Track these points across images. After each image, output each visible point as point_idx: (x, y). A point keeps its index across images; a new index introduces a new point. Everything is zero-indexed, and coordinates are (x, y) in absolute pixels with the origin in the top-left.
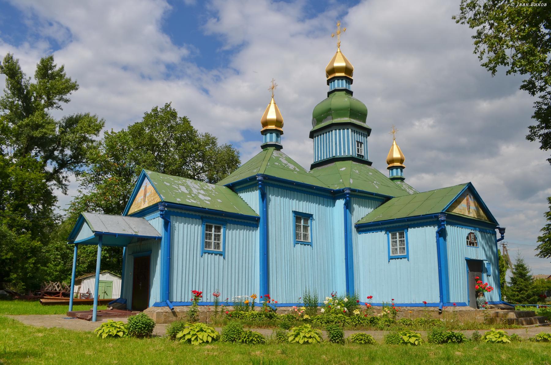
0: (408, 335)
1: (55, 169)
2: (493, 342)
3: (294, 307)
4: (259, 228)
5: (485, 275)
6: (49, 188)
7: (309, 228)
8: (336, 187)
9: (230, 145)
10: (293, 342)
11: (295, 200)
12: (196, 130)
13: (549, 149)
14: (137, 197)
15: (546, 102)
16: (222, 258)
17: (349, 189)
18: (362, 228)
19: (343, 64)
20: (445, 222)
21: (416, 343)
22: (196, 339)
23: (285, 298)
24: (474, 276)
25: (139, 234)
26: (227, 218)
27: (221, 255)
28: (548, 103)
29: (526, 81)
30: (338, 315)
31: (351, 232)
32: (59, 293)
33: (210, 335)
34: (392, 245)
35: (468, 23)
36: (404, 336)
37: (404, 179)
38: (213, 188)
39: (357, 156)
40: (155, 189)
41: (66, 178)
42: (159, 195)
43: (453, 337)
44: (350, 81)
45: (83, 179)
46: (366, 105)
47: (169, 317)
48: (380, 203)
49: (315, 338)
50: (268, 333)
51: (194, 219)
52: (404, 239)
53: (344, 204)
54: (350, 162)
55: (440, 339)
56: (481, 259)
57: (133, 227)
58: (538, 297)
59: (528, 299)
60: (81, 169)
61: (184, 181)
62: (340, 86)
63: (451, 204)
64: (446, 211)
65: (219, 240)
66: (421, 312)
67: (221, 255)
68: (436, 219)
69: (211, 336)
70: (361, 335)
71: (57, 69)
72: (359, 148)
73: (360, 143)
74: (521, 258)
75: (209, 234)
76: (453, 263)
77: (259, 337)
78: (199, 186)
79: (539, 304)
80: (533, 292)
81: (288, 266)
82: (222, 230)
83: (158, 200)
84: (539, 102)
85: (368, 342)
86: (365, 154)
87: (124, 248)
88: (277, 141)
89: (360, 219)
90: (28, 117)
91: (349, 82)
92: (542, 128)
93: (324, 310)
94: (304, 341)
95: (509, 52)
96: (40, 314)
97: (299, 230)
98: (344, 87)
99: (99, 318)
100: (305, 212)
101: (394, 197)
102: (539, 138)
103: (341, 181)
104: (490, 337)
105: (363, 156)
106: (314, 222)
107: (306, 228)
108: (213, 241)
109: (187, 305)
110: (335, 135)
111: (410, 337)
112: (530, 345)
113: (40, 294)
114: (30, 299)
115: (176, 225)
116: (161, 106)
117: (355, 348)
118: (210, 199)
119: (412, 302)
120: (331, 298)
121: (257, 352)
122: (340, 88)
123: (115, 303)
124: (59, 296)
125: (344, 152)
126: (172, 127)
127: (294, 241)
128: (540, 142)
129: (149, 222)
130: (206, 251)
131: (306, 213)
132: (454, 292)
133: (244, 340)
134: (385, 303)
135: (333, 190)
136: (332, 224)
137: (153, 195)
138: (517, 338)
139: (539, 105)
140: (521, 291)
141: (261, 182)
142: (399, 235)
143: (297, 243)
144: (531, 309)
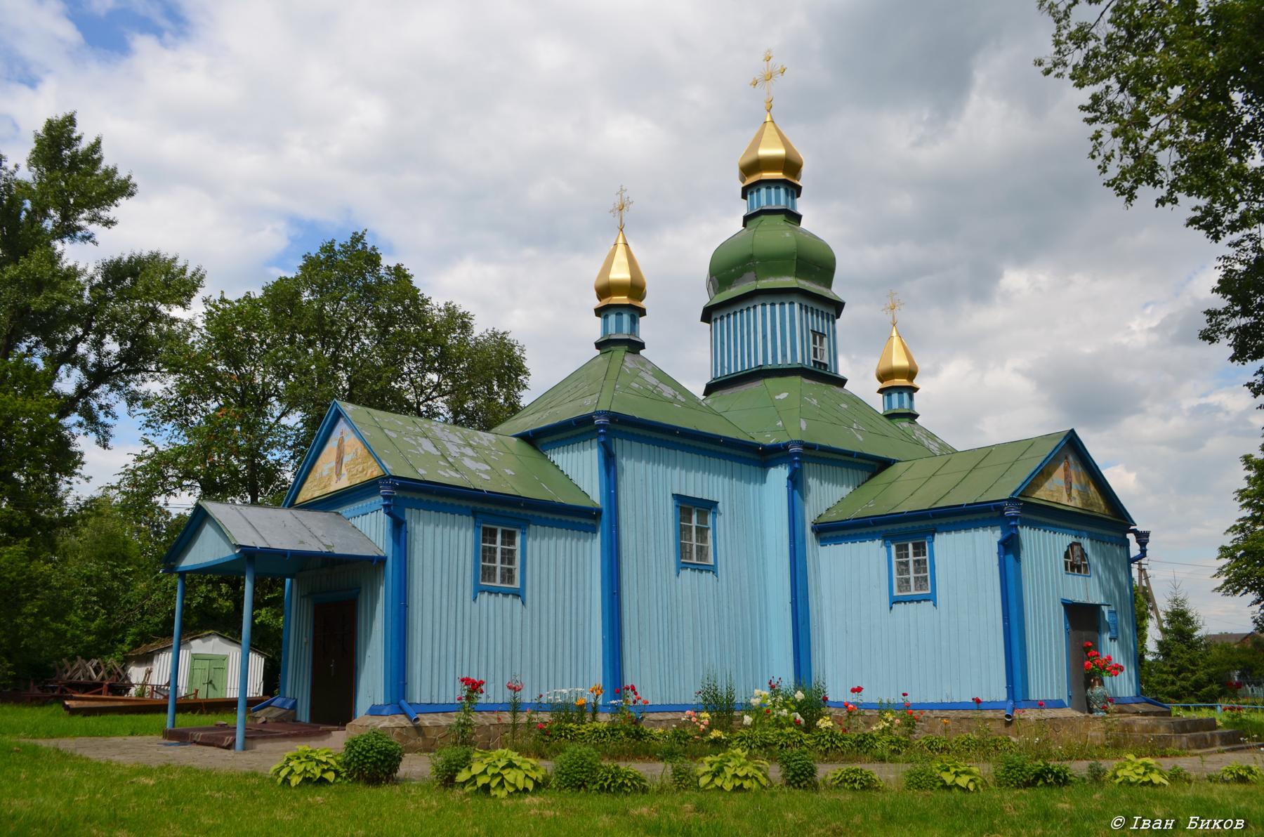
0: (953, 770)
1: (80, 387)
2: (1131, 784)
3: (688, 712)
4: (599, 534)
6: (66, 433)
7: (710, 533)
8: (770, 439)
9: (504, 333)
10: (710, 787)
11: (678, 469)
12: (426, 296)
13: (1249, 361)
14: (319, 463)
15: (1243, 258)
16: (519, 601)
17: (800, 444)
18: (830, 531)
19: (780, 152)
20: (1018, 520)
21: (971, 786)
22: (501, 785)
23: (659, 693)
25: (337, 551)
26: (529, 513)
28: (1249, 260)
29: (1200, 209)
30: (784, 728)
32: (99, 685)
33: (530, 775)
34: (898, 570)
35: (1072, 77)
36: (944, 773)
37: (916, 416)
38: (490, 441)
39: (812, 365)
40: (366, 445)
41: (107, 409)
42: (378, 461)
43: (1047, 774)
44: (795, 191)
45: (151, 413)
46: (834, 252)
47: (407, 738)
48: (867, 474)
49: (756, 779)
50: (654, 771)
51: (457, 515)
52: (924, 557)
53: (788, 478)
54: (797, 380)
55: (1021, 777)
56: (1097, 603)
57: (319, 533)
58: (1220, 687)
59: (1196, 690)
60: (143, 389)
61: (425, 425)
62: (773, 203)
63: (1031, 479)
64: (1020, 495)
65: (511, 562)
66: (966, 722)
68: (997, 514)
69: (531, 779)
70: (853, 771)
71: (83, 146)
72: (818, 346)
73: (818, 335)
74: (1181, 597)
75: (490, 548)
76: (1035, 612)
77: (635, 778)
78: (460, 438)
79: (1222, 704)
80: (1208, 674)
81: (665, 620)
82: (518, 539)
83: (374, 472)
84: (1228, 258)
85: (868, 785)
86: (830, 361)
87: (288, 581)
89: (824, 513)
90: (16, 262)
91: (792, 192)
92: (1234, 315)
93: (751, 719)
94: (734, 786)
95: (1167, 158)
96: (98, 736)
97: (688, 537)
98: (782, 205)
99: (249, 742)
100: (700, 497)
101: (899, 461)
102: (1227, 337)
103: (780, 423)
104: (1126, 773)
105: (825, 365)
106: (719, 519)
107: (702, 532)
108: (498, 564)
109: (444, 709)
110: (760, 316)
111: (957, 774)
112: (1211, 790)
113: (53, 689)
114: (32, 699)
116: (343, 239)
117: (846, 797)
119: (945, 700)
120: (766, 693)
121: (642, 809)
122: (773, 206)
123: (268, 709)
124: (100, 693)
125: (784, 355)
126: (368, 288)
128: (1230, 345)
129: (353, 521)
131: (702, 499)
132: (1038, 677)
133: (606, 785)
134: (885, 701)
135: (763, 446)
137: (360, 460)
138: (1183, 776)
139: (1229, 263)
140: (1180, 672)
142: (914, 549)
143: (682, 568)
144: (1204, 714)
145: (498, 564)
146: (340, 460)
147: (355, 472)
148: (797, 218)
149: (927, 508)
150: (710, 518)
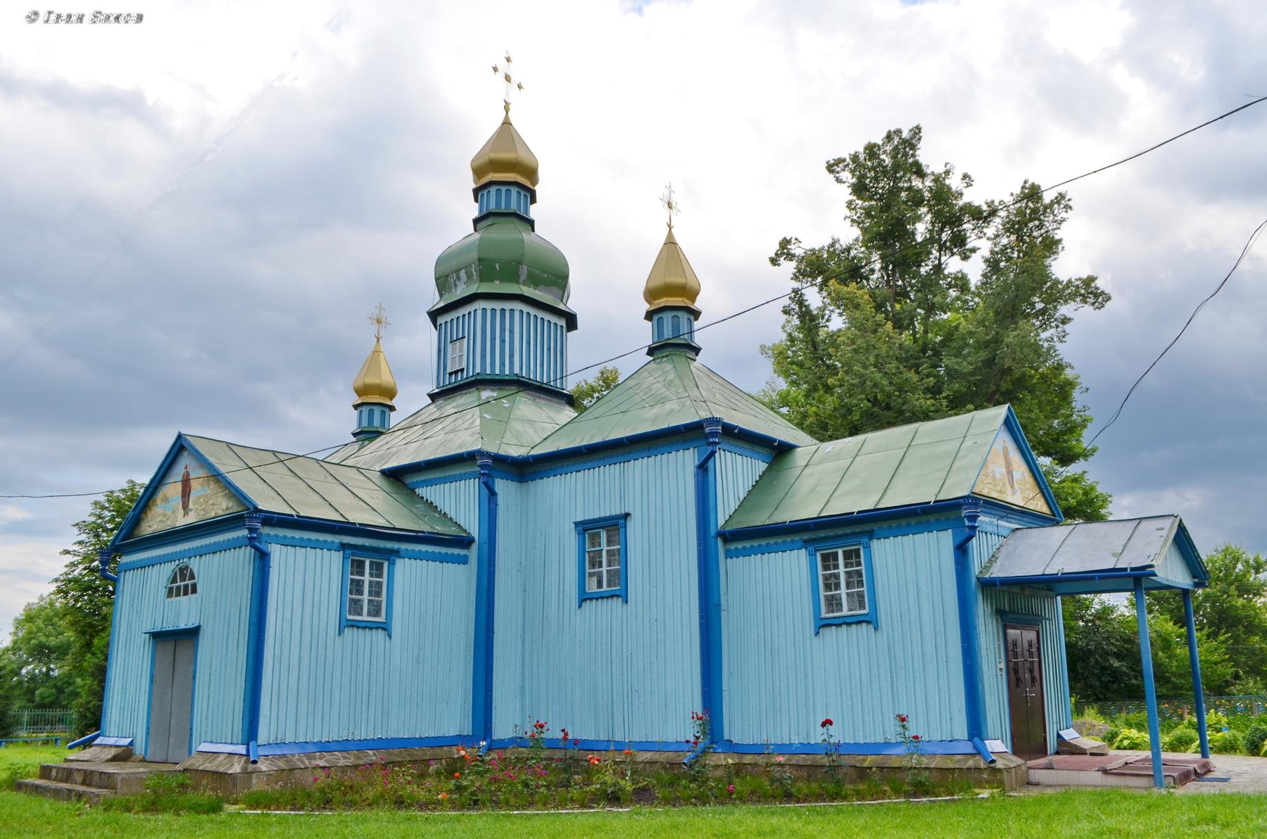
65: (379, 594)
122: (503, 208)
125: (502, 364)
148: (531, 223)
149: (815, 516)
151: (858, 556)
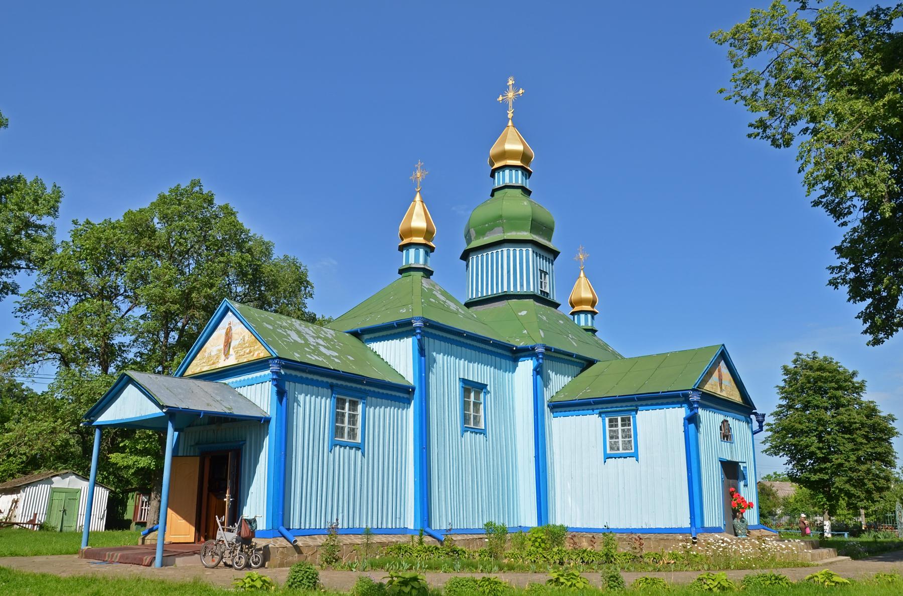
5: (742, 483)
7: (482, 406)
16: (359, 453)
18: (558, 407)
24: (729, 487)
27: (358, 448)
31: (543, 414)
37: (596, 331)
39: (539, 293)
48: (579, 369)
52: (629, 427)
53: (533, 370)
56: (737, 461)
65: (354, 424)
66: (662, 542)
67: (358, 448)
82: (360, 407)
83: (261, 353)
88: (426, 261)
98: (520, 183)
103: (525, 331)
105: (547, 294)
107: (477, 405)
108: (346, 424)
115: (301, 398)
118: (337, 355)
122: (514, 183)
125: (522, 285)
127: (462, 427)
130: (337, 443)
131: (477, 383)
135: (516, 347)
136: (512, 401)
141: (420, 330)
145: (346, 424)
146: (228, 344)
147: (242, 353)
150: (482, 395)
151: (629, 420)
